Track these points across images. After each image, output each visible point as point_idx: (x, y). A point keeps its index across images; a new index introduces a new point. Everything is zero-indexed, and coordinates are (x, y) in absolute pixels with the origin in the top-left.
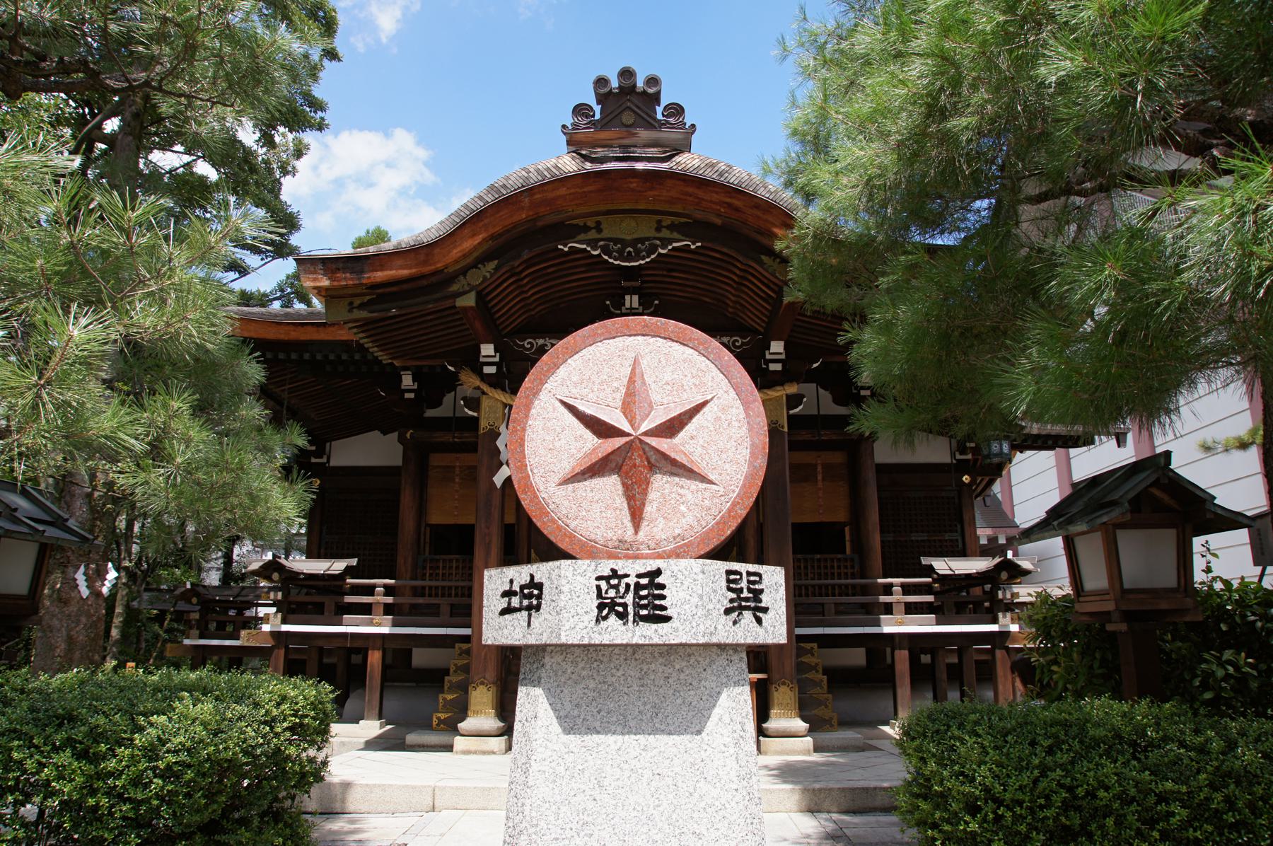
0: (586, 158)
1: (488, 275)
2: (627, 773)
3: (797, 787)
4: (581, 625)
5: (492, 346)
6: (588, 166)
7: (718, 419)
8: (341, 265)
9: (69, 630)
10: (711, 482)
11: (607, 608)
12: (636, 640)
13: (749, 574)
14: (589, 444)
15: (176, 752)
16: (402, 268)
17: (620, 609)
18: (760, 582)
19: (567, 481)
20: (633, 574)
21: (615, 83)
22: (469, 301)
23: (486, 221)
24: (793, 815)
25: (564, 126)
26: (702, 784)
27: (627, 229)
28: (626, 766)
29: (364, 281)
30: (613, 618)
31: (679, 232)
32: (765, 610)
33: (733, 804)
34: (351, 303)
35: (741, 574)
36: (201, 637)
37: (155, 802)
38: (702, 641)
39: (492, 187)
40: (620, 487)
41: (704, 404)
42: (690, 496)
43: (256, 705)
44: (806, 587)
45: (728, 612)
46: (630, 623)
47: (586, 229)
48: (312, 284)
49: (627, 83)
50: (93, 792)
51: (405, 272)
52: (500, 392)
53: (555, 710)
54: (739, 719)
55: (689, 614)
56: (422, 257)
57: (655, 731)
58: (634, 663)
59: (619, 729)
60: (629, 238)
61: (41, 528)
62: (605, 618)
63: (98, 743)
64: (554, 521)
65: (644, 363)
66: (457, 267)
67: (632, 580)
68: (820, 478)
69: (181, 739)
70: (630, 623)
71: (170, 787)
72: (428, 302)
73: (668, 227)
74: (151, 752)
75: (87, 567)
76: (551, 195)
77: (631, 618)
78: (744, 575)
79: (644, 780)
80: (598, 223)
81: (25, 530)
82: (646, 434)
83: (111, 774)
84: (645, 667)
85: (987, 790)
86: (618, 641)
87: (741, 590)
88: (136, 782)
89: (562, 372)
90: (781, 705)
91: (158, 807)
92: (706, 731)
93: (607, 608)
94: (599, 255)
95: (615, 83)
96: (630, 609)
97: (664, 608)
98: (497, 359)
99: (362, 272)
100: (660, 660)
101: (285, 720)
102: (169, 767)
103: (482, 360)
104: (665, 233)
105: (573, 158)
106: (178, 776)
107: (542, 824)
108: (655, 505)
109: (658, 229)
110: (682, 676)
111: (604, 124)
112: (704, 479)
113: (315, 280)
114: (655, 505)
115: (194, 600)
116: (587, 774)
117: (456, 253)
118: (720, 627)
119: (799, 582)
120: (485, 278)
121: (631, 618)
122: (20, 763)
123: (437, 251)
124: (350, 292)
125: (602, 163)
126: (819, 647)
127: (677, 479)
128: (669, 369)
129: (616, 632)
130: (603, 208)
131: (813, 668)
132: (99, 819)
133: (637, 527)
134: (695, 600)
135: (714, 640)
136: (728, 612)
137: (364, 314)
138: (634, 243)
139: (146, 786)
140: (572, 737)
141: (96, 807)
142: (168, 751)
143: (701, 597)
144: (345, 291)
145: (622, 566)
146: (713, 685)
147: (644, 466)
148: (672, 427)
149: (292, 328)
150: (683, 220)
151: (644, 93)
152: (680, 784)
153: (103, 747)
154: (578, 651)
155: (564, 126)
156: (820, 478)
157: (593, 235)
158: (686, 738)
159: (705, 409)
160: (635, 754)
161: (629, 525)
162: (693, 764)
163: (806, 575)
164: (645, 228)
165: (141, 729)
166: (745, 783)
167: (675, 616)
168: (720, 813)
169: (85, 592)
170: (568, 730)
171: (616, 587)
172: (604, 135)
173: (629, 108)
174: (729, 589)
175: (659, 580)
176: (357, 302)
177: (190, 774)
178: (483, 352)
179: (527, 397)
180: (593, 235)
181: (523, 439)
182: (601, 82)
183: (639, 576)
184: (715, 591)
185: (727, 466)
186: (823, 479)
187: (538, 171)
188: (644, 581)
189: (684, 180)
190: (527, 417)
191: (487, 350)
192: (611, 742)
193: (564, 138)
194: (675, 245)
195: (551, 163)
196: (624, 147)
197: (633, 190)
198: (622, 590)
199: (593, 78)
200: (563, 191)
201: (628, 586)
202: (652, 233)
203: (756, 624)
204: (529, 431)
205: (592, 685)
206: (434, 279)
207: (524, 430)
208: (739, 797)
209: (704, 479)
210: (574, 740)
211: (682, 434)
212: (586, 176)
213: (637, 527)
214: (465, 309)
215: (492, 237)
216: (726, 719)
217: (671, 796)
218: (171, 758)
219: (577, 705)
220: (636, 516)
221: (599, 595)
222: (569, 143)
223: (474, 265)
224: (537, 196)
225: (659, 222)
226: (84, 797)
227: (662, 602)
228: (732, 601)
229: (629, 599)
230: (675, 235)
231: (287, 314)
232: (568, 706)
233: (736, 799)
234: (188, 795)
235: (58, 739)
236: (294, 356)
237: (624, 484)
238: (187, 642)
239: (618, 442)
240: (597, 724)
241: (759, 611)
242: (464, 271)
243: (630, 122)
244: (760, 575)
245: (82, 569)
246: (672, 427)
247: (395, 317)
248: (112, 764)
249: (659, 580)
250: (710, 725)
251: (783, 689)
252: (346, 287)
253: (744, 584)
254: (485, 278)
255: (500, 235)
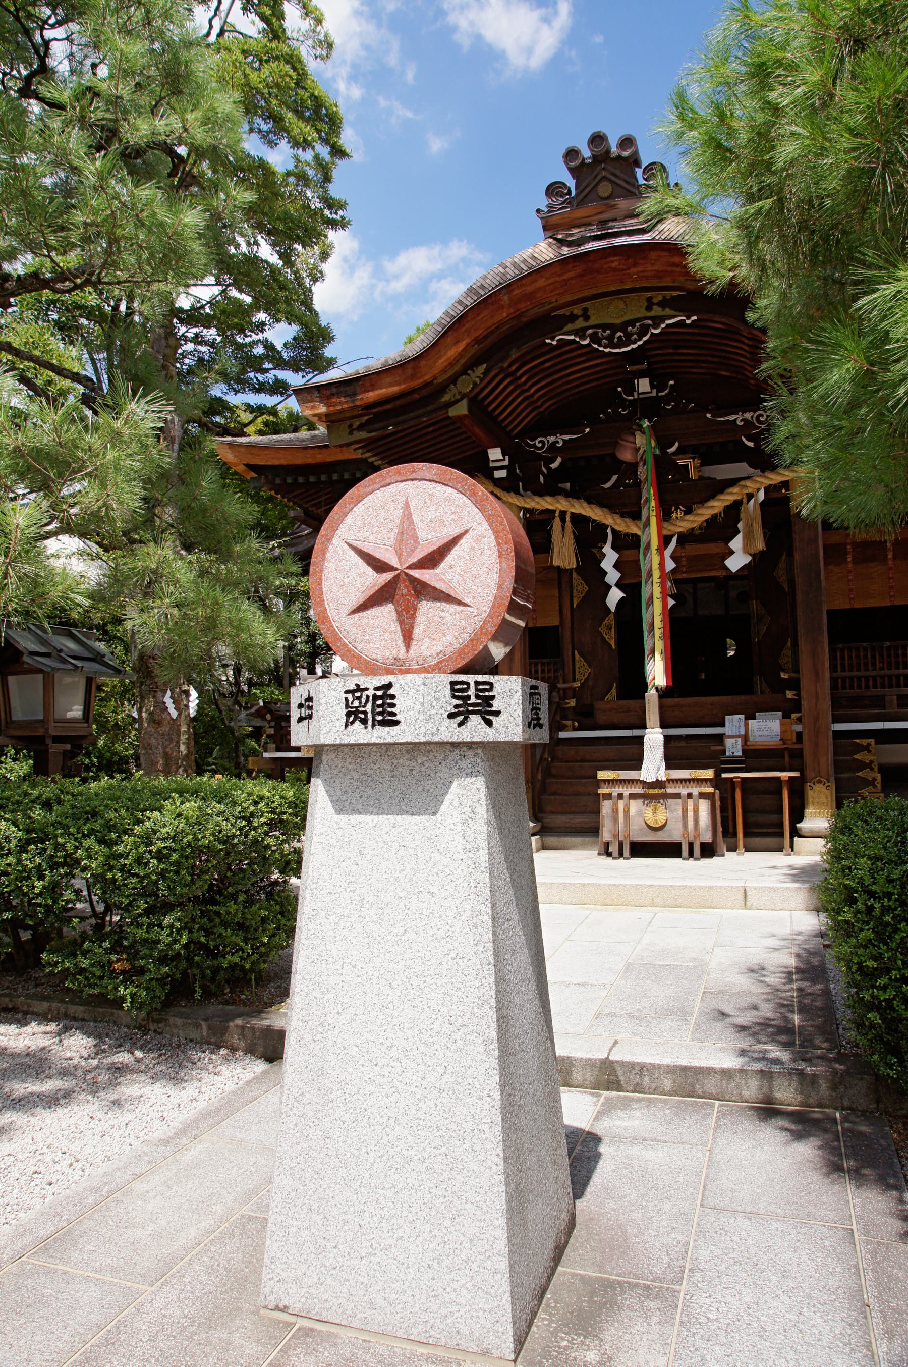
0: (561, 242)
1: (478, 380)
2: (381, 845)
3: (807, 886)
4: (334, 730)
5: (499, 450)
6: (565, 251)
7: (473, 548)
8: (334, 390)
9: (165, 748)
10: (465, 605)
11: (353, 715)
12: (374, 740)
13: (477, 683)
14: (374, 580)
15: (164, 839)
16: (391, 385)
17: (362, 716)
18: (491, 690)
19: (354, 612)
20: (371, 688)
21: (586, 153)
22: (461, 409)
23: (467, 326)
24: (797, 914)
25: (538, 211)
26: (436, 854)
27: (613, 313)
28: (379, 839)
29: (358, 403)
30: (357, 723)
31: (671, 308)
32: (497, 713)
33: (459, 870)
34: (350, 426)
35: (468, 684)
36: (278, 750)
37: (154, 877)
38: (423, 740)
39: (471, 289)
40: (394, 614)
41: (454, 541)
42: (449, 618)
43: (234, 803)
44: (867, 678)
45: (451, 716)
46: (370, 727)
47: (573, 318)
48: (311, 412)
49: (600, 150)
50: (111, 868)
51: (395, 389)
52: (512, 494)
53: (330, 796)
54: (470, 803)
55: (413, 718)
56: (409, 371)
57: (401, 812)
58: (387, 759)
59: (375, 811)
60: (618, 321)
61: (79, 663)
62: (352, 723)
63: (110, 831)
64: (345, 645)
65: (412, 505)
66: (446, 377)
67: (370, 693)
68: (890, 556)
69: (166, 829)
70: (370, 727)
71: (162, 866)
72: (423, 415)
73: (660, 304)
74: (147, 839)
75: (172, 692)
76: (529, 289)
77: (370, 723)
78: (472, 685)
79: (393, 850)
80: (585, 310)
81: (70, 667)
82: (410, 567)
83: (121, 856)
84: (395, 762)
85: (861, 882)
86: (361, 742)
87: (469, 697)
88: (139, 861)
89: (349, 519)
90: (819, 804)
91: (156, 882)
92: (440, 813)
93: (353, 715)
94: (589, 345)
95: (586, 153)
96: (370, 716)
97: (394, 714)
98: (506, 463)
99: (355, 394)
100: (407, 756)
101: (262, 816)
102: (160, 851)
103: (491, 465)
104: (657, 311)
105: (550, 245)
106: (167, 857)
107: (320, 881)
108: (422, 627)
109: (649, 308)
110: (423, 769)
111: (582, 199)
112: (460, 603)
113: (313, 408)
114: (422, 627)
115: (268, 717)
116: (352, 845)
117: (441, 363)
118: (442, 729)
119: (835, 675)
120: (475, 384)
121: (370, 723)
122: (63, 845)
123: (423, 363)
124: (348, 414)
125: (579, 246)
126: (876, 743)
127: (438, 604)
128: (433, 508)
129: (360, 734)
130: (586, 293)
131: (869, 765)
132: (118, 888)
133: (408, 646)
134: (418, 707)
135: (436, 739)
136: (451, 716)
137: (363, 435)
138: (623, 327)
139: (147, 864)
140: (341, 816)
141: (114, 880)
142: (158, 839)
143: (422, 704)
144: (342, 416)
145: (364, 682)
146: (447, 775)
147: (411, 595)
148: (433, 559)
149: (317, 451)
150: (675, 293)
151: (619, 157)
152: (419, 854)
153: (113, 835)
154: (346, 750)
155: (538, 211)
156: (890, 556)
157: (580, 323)
158: (424, 818)
159: (462, 541)
160: (387, 830)
161: (402, 645)
162: (429, 839)
163: (874, 664)
164: (635, 309)
165: (139, 822)
166: (471, 855)
167: (402, 720)
168: (450, 877)
169: (174, 713)
170: (339, 811)
171: (359, 698)
172: (581, 213)
173: (605, 178)
174: (454, 697)
175: (391, 692)
176: (356, 424)
177: (175, 857)
178: (492, 458)
179: (323, 543)
180: (580, 323)
181: (321, 579)
182: (571, 154)
183: (376, 689)
184: (437, 699)
185: (480, 590)
186: (894, 558)
187: (514, 264)
188: (380, 693)
189: (669, 250)
190: (323, 560)
191: (495, 454)
192: (369, 820)
193: (539, 224)
194: (668, 322)
195: (526, 253)
196: (603, 223)
197: (615, 270)
198: (363, 700)
199: (563, 151)
200: (542, 282)
201: (368, 697)
202: (643, 313)
203: (484, 725)
204: (325, 571)
205: (356, 776)
206: (424, 392)
207: (321, 571)
208: (463, 865)
209: (460, 603)
210: (343, 818)
211: (442, 565)
212: (564, 262)
213: (408, 646)
214: (460, 418)
215: (477, 341)
216: (456, 803)
217: (412, 863)
218: (160, 844)
219: (345, 792)
220: (408, 637)
221: (347, 706)
222: (545, 228)
223: (464, 372)
224: (517, 292)
225: (649, 299)
226: (105, 872)
227: (393, 710)
228: (456, 707)
229: (369, 708)
230: (668, 312)
231: (313, 437)
232: (339, 793)
233: (462, 867)
234: (177, 873)
235: (85, 829)
236: (323, 478)
237: (397, 611)
238: (266, 755)
239: (388, 576)
240: (360, 807)
241: (488, 714)
242: (454, 380)
243: (606, 195)
244: (491, 684)
245: (169, 693)
246: (433, 559)
247: (393, 434)
248: (120, 849)
249: (391, 692)
250: (443, 808)
251: (818, 787)
252: (343, 411)
253: (472, 692)
254: (475, 384)
255: (486, 337)
